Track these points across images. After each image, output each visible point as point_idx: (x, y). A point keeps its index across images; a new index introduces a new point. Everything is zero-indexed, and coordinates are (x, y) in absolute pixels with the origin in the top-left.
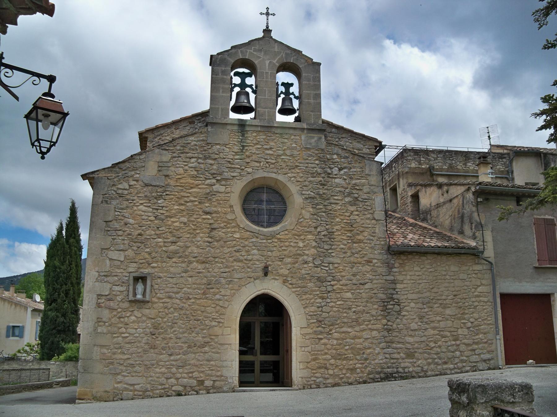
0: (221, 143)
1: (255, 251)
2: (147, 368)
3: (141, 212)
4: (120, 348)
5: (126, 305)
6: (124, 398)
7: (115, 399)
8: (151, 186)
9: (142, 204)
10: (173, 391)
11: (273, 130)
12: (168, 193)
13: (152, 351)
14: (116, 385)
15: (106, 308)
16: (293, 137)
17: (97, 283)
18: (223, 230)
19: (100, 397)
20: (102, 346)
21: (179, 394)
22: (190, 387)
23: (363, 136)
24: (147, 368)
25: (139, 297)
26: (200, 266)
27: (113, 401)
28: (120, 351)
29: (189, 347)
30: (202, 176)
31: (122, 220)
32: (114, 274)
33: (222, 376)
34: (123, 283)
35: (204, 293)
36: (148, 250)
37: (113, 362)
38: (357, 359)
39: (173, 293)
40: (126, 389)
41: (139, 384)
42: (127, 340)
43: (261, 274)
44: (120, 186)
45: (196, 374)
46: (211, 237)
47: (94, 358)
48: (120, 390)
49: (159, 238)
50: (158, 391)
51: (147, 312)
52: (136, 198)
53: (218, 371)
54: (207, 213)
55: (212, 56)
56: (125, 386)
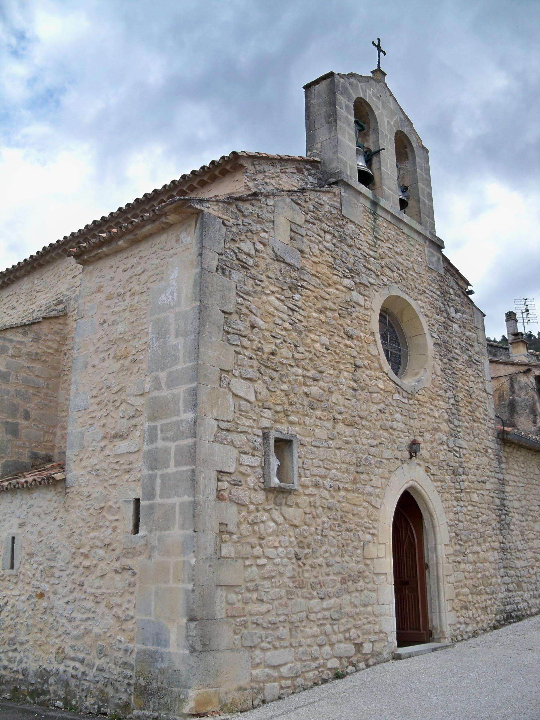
0: (356, 222)
1: (398, 416)
2: (294, 627)
3: (273, 309)
4: (256, 589)
5: (260, 496)
6: (268, 698)
7: (256, 703)
8: (284, 262)
9: (273, 292)
10: (329, 669)
11: (402, 226)
12: (305, 284)
13: (299, 592)
14: (254, 672)
15: (231, 501)
16: (417, 246)
17: (216, 445)
18: (368, 372)
19: (232, 704)
20: (229, 587)
21: (339, 676)
22: (346, 657)
23: (457, 271)
24: (294, 627)
25: (275, 481)
26: (348, 431)
27: (254, 707)
28: (255, 596)
29: (343, 581)
30: (340, 269)
31: (247, 316)
32: (241, 429)
33: (381, 632)
34: (254, 449)
35: (354, 482)
36: (284, 387)
37: (246, 622)
38: (487, 593)
39: (320, 476)
40: (269, 678)
41: (285, 664)
42: (265, 571)
43: (407, 454)
44: (242, 246)
45: (353, 633)
46: (355, 381)
47: (218, 616)
48: (259, 682)
49: (298, 366)
50: (311, 674)
51: (290, 512)
52: (264, 278)
53: (375, 623)
54: (350, 337)
55: (385, 75)
56: (267, 670)
